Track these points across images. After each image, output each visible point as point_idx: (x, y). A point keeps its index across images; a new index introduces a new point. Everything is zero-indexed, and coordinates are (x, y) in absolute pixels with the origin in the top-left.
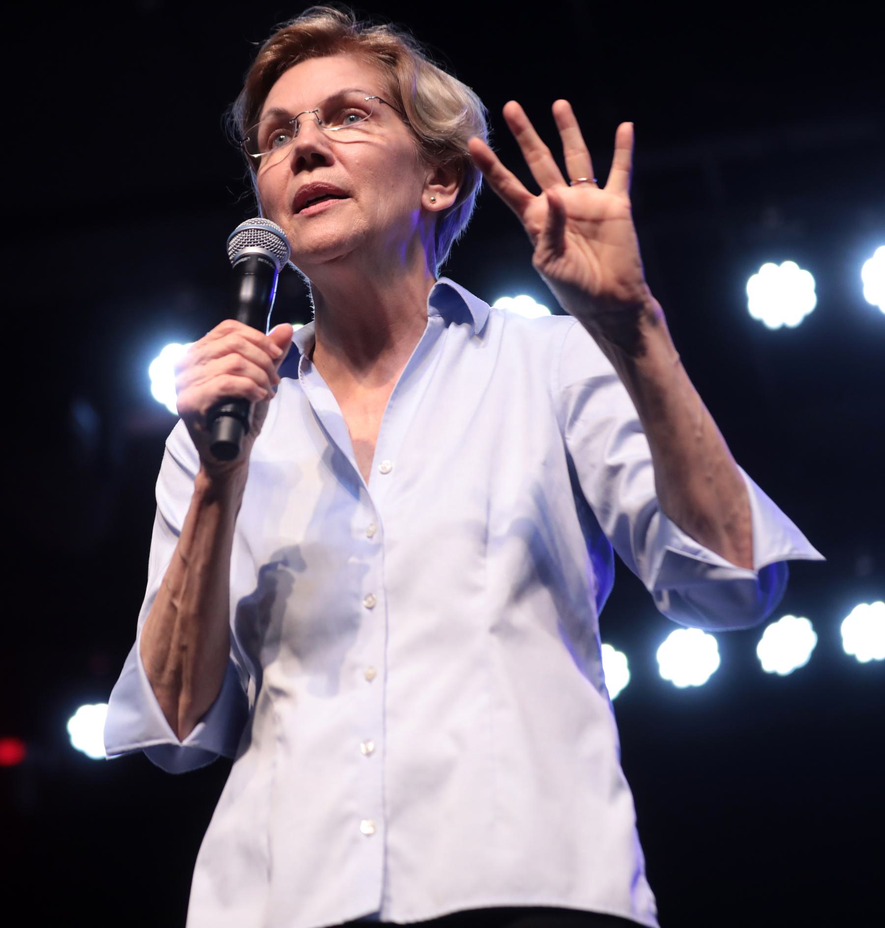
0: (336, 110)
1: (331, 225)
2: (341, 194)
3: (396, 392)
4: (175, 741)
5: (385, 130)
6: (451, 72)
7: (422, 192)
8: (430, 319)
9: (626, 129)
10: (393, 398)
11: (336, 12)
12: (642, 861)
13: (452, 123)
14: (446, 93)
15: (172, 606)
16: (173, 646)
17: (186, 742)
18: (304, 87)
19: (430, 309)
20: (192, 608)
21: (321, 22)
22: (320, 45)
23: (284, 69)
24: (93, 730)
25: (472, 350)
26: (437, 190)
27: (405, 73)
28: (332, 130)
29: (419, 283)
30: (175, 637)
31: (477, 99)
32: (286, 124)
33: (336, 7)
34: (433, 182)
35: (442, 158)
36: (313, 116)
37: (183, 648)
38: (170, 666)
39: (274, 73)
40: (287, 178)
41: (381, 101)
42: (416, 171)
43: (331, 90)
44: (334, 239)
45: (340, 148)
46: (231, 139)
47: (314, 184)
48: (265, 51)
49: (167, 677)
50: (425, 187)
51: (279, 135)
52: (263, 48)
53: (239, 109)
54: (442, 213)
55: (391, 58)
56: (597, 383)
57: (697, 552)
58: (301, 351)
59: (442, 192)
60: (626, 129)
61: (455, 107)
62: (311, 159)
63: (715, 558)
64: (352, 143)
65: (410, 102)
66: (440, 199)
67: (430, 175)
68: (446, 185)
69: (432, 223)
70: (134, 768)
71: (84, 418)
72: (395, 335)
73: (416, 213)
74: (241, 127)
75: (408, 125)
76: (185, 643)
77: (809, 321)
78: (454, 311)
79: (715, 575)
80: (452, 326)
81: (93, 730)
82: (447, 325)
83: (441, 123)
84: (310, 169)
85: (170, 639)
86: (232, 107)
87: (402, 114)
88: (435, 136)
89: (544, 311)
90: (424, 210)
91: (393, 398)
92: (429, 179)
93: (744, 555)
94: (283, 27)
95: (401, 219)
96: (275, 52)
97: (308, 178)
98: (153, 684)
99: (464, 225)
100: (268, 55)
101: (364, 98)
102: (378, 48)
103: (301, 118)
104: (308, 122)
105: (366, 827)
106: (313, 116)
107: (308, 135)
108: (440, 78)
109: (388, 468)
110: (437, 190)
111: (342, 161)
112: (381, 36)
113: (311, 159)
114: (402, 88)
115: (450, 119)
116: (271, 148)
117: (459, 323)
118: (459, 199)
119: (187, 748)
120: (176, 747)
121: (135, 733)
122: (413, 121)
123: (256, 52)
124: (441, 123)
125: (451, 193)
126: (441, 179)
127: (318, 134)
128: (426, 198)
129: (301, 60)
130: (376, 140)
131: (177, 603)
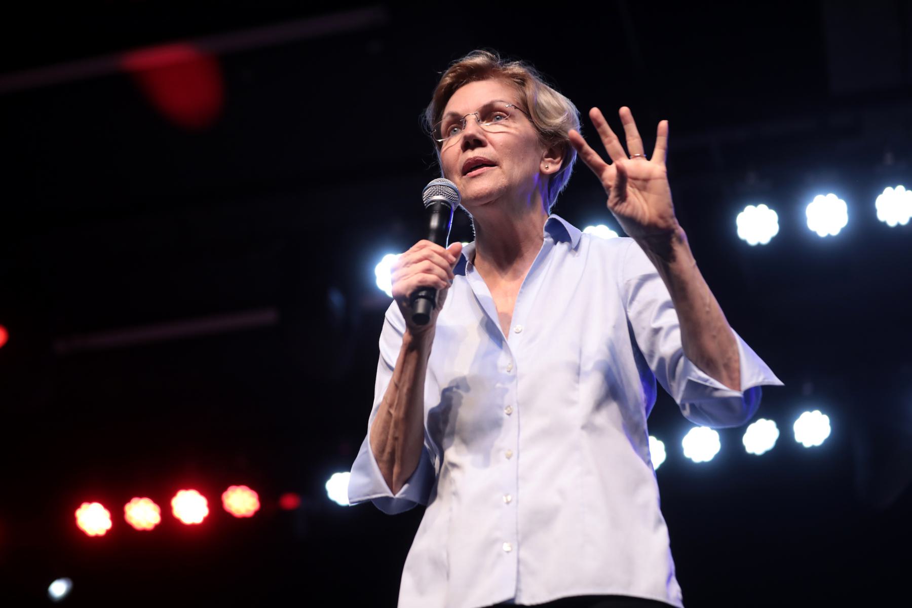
0: (488, 113)
1: (485, 183)
3: (525, 283)
4: (390, 494)
5: (517, 125)
9: (663, 124)
10: (523, 287)
12: (673, 567)
13: (558, 121)
14: (555, 103)
15: (389, 413)
16: (390, 437)
17: (398, 496)
18: (469, 98)
19: (545, 234)
20: (401, 414)
21: (479, 59)
22: (479, 73)
23: (457, 88)
24: (341, 488)
25: (572, 260)
27: (529, 91)
28: (486, 125)
29: (539, 217)
30: (391, 431)
31: (573, 106)
32: (458, 121)
33: (488, 50)
34: (547, 157)
35: (552, 142)
36: (474, 117)
37: (395, 439)
38: (388, 449)
39: (450, 91)
40: (459, 154)
41: (516, 108)
42: (537, 150)
43: (485, 100)
45: (491, 136)
47: (475, 158)
49: (386, 456)
50: (542, 159)
53: (429, 112)
54: (553, 175)
55: (521, 82)
56: (646, 278)
57: (706, 381)
58: (467, 259)
59: (552, 163)
60: (663, 124)
61: (561, 111)
62: (471, 143)
63: (717, 384)
64: (498, 134)
65: (533, 108)
66: (551, 167)
67: (545, 152)
68: (555, 158)
69: (547, 182)
70: (366, 511)
71: (336, 299)
72: (524, 249)
73: (537, 175)
74: (431, 123)
75: (532, 122)
76: (397, 435)
77: (774, 240)
78: (560, 235)
79: (717, 394)
80: (559, 243)
81: (341, 488)
82: (555, 243)
83: (552, 121)
84: (473, 149)
85: (388, 433)
87: (528, 116)
88: (548, 129)
89: (614, 234)
90: (542, 174)
91: (523, 287)
93: (735, 382)
95: (527, 179)
96: (452, 78)
97: (471, 154)
98: (377, 461)
99: (566, 183)
100: (447, 80)
102: (514, 76)
103: (467, 118)
104: (471, 120)
105: (506, 547)
106: (474, 117)
107: (471, 128)
111: (491, 144)
112: (515, 68)
113: (471, 143)
117: (563, 242)
118: (563, 167)
119: (398, 499)
120: (392, 498)
121: (366, 490)
122: (535, 120)
123: (440, 77)
125: (558, 163)
126: (552, 154)
128: (543, 166)
129: (467, 83)
130: (513, 131)
131: (392, 411)
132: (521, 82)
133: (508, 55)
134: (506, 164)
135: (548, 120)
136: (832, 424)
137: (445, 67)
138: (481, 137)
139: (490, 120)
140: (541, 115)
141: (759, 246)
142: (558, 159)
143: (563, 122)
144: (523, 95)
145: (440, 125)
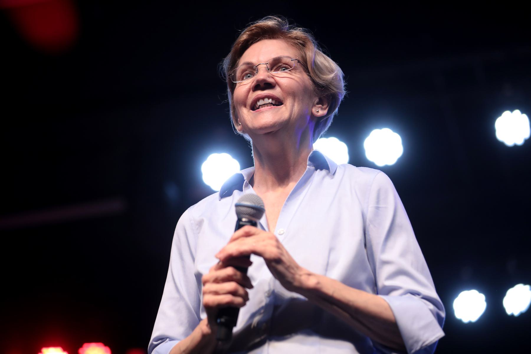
0: (276, 64)
1: (267, 117)
2: (278, 102)
6: (328, 56)
7: (312, 107)
8: (308, 167)
10: (287, 201)
11: (280, 20)
14: (327, 64)
18: (262, 53)
19: (308, 162)
21: (270, 23)
23: (252, 43)
25: (328, 179)
26: (319, 107)
28: (273, 73)
32: (252, 69)
33: (279, 17)
34: (318, 104)
36: (265, 66)
39: (246, 45)
40: (249, 92)
41: (299, 62)
42: (310, 97)
43: (274, 56)
44: (271, 123)
46: (221, 75)
48: (243, 35)
50: (314, 105)
51: (247, 74)
52: (242, 33)
53: (226, 62)
55: (304, 45)
58: (245, 178)
59: (322, 109)
61: (331, 71)
64: (284, 78)
65: (311, 64)
67: (317, 100)
68: (323, 105)
72: (292, 173)
74: (226, 72)
75: (310, 76)
80: (318, 170)
82: (316, 170)
83: (324, 77)
84: (263, 89)
86: (223, 60)
87: (306, 70)
88: (321, 82)
90: (312, 115)
91: (287, 201)
92: (316, 102)
94: (252, 24)
95: (301, 116)
97: (260, 93)
100: (244, 37)
101: (288, 60)
102: (296, 38)
103: (259, 67)
106: (265, 66)
107: (262, 75)
108: (325, 58)
109: (282, 232)
110: (319, 107)
112: (298, 32)
114: (308, 59)
115: (329, 75)
116: (243, 79)
117: (321, 170)
122: (312, 74)
124: (324, 77)
125: (325, 109)
127: (267, 74)
128: (314, 110)
130: (296, 79)
132: (302, 45)
133: (295, 22)
134: (289, 102)
135: (321, 76)
136: (487, 300)
137: (244, 26)
138: (271, 80)
139: (277, 70)
140: (316, 71)
141: (470, 324)
142: (325, 106)
143: (333, 79)
144: (304, 55)
145: (235, 72)
